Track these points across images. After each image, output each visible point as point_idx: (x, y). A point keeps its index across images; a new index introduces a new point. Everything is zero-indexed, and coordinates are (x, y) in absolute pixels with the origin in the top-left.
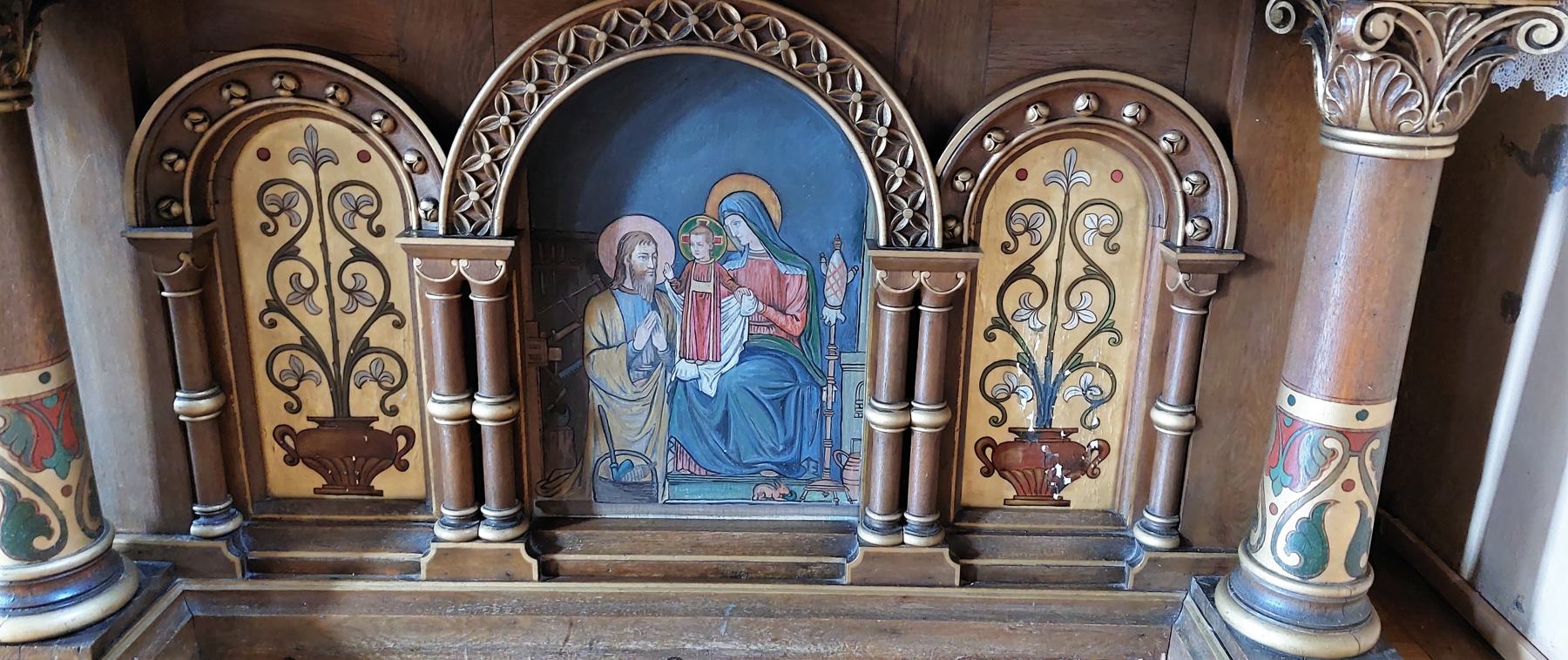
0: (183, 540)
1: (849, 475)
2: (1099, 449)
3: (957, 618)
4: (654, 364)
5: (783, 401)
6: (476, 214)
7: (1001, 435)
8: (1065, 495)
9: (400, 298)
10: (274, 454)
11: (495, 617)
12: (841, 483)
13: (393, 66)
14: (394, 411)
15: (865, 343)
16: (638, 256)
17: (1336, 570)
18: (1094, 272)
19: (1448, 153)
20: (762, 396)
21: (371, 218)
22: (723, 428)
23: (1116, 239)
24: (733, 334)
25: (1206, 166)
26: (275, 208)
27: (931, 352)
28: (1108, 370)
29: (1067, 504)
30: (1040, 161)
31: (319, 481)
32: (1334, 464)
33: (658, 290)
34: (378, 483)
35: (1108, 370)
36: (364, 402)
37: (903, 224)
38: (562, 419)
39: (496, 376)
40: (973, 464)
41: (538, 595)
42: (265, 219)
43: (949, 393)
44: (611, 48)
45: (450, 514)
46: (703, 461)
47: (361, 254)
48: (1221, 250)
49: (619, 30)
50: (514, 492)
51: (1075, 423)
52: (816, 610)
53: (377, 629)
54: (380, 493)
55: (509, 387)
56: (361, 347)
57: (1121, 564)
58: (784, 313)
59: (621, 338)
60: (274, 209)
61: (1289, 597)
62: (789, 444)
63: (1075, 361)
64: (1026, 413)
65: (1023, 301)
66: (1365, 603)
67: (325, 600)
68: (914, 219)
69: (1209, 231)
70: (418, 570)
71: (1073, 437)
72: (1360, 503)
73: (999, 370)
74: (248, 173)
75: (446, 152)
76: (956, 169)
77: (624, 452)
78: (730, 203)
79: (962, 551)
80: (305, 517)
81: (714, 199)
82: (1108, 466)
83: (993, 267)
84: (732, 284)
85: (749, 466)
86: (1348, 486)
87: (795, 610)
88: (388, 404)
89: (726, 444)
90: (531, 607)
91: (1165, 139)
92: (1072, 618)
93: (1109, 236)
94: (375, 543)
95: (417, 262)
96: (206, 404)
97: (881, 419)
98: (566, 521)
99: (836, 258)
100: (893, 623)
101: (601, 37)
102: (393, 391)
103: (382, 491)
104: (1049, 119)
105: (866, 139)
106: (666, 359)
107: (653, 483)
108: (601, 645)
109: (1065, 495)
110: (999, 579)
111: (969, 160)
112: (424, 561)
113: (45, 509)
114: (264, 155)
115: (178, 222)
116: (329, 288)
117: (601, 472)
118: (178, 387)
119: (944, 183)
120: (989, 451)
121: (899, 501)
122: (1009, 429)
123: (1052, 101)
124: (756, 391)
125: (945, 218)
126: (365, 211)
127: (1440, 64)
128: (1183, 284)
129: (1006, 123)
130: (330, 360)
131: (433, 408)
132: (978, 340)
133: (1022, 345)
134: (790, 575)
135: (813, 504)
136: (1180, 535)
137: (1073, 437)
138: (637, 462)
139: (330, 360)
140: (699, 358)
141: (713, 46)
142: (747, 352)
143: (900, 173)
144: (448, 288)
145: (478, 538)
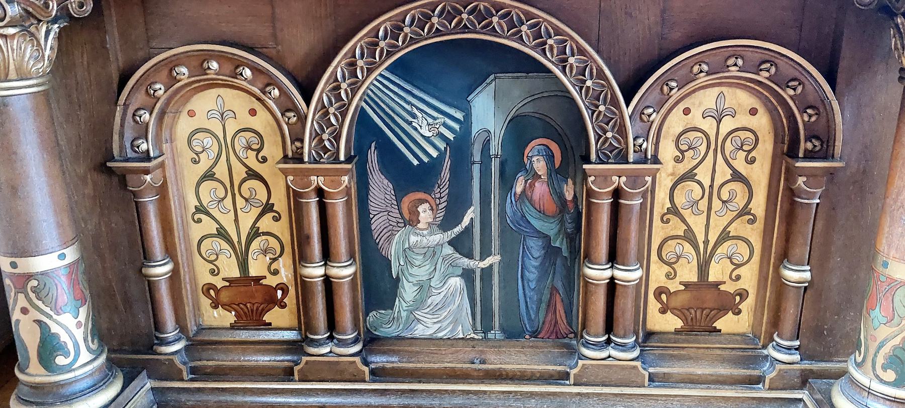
14: (276, 273)
21: (749, 152)
36: (717, 272)
70: (568, 378)
88: (273, 267)
91: (160, 89)
95: (290, 178)
103: (721, 330)
120: (664, 297)
122: (223, 279)
123: (199, 63)
128: (151, 182)
139: (235, 239)
141: (426, 39)
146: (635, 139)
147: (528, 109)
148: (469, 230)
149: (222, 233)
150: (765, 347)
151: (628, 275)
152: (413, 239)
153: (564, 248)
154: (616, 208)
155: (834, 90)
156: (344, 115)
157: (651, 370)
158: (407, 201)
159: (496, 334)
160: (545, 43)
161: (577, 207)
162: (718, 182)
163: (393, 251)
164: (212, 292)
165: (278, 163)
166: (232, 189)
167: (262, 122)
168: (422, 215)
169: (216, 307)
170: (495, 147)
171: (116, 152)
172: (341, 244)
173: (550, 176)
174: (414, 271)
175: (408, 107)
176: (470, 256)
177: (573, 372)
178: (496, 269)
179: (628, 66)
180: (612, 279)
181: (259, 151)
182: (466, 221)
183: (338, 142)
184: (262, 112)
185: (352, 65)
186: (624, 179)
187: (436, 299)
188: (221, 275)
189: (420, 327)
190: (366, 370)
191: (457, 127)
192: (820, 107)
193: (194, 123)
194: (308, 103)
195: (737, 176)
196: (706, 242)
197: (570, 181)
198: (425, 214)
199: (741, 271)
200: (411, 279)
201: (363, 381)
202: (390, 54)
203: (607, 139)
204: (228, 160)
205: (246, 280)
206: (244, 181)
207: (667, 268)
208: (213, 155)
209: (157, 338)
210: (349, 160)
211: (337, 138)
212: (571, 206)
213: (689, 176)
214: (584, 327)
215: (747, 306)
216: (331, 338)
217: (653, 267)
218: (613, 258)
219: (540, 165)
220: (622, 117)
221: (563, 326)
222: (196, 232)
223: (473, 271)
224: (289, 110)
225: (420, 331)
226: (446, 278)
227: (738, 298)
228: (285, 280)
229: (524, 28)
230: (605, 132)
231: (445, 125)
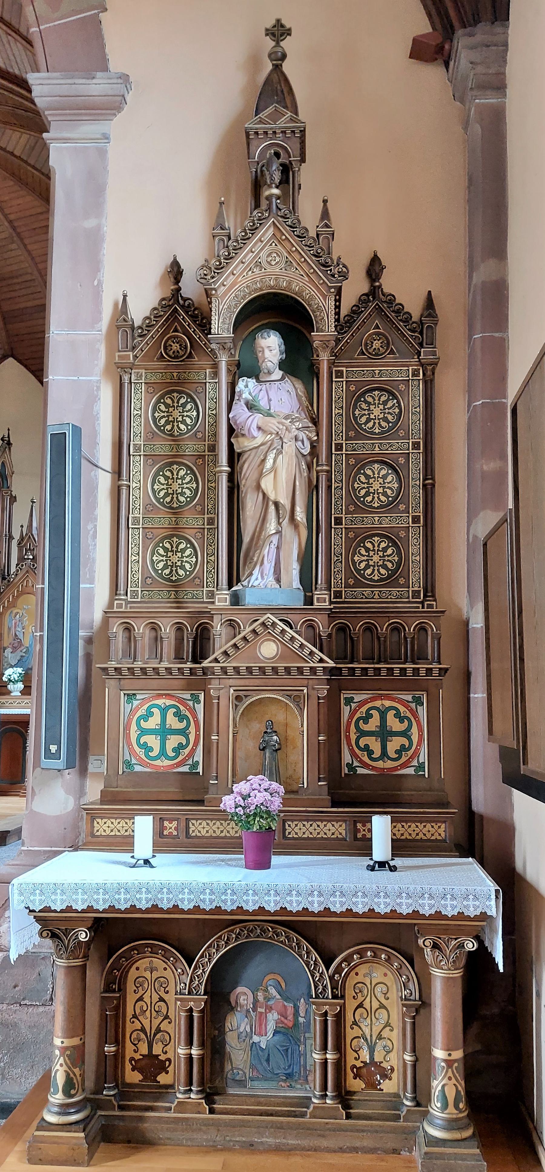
0: (100, 1097)
1: (310, 1078)
2: (391, 1069)
3: (343, 1131)
4: (246, 1037)
5: (287, 1050)
6: (197, 987)
7: (359, 1064)
8: (382, 1087)
9: (171, 1014)
10: (128, 1067)
11: (195, 1127)
12: (307, 1081)
13: (176, 944)
15: (312, 1030)
16: (242, 1000)
17: (451, 1108)
18: (382, 1006)
19: (461, 974)
20: (280, 1048)
21: (165, 988)
22: (268, 1060)
23: (388, 995)
24: (271, 1026)
25: (408, 973)
26: (138, 984)
27: (332, 1033)
28: (390, 1040)
29: (382, 1090)
30: (363, 970)
31: (141, 1077)
32: (445, 1071)
33: (248, 1011)
34: (159, 1078)
35: (390, 1040)
36: (157, 1049)
37: (320, 991)
38: (217, 1056)
39: (198, 1040)
40: (350, 1075)
41: (208, 1119)
42: (135, 988)
43: (339, 1048)
44: (237, 938)
45: (182, 1089)
46: (261, 1072)
47: (161, 999)
48: (415, 1000)
49: (239, 934)
50: (201, 1083)
51: (382, 1060)
52: (299, 1127)
53: (158, 1130)
54: (159, 1082)
55: (202, 1045)
56: (158, 1030)
57: (400, 1112)
58: (286, 1018)
59: (236, 1027)
60: (138, 985)
61: (443, 1119)
62: (289, 1066)
63: (380, 1037)
64: (366, 1055)
65: (361, 1015)
66: (466, 1121)
67: (141, 1119)
68: (323, 989)
69: (411, 994)
71: (381, 1065)
73: (356, 1040)
74: (133, 974)
75: (190, 969)
76: (336, 972)
77: (236, 1068)
78: (270, 983)
79: (346, 1106)
80: (136, 1090)
81: (265, 981)
82: (394, 1076)
83: (351, 1005)
84: (270, 1009)
85: (277, 1074)
87: (290, 1127)
89: (269, 1066)
90: (206, 1123)
92: (382, 1132)
93: (385, 994)
94: (157, 1100)
96: (113, 1049)
97: (317, 1056)
98: (218, 1094)
99: (302, 1000)
100: (322, 1132)
101: (234, 936)
102: (166, 1045)
104: (360, 958)
105: (308, 964)
106: (249, 1034)
107: (245, 1080)
108: (228, 1138)
109: (382, 1087)
110: (359, 1117)
111: (339, 970)
112: (173, 1106)
113: (75, 1081)
114: (137, 969)
115: (114, 991)
116: (151, 1010)
117: (229, 1076)
118: (106, 1043)
119: (331, 978)
120: (355, 1070)
121: (324, 1088)
123: (361, 953)
124: (278, 1047)
125: (332, 989)
126: (164, 986)
127: (448, 952)
129: (348, 959)
130: (149, 1035)
131: (180, 1051)
132: (348, 1029)
133: (362, 1031)
134: (289, 1114)
135: (297, 1089)
136: (417, 1101)
137: (381, 1065)
138: (240, 1072)
139: (149, 1035)
140: (260, 1035)
142: (276, 1032)
143: (318, 975)
144: (187, 1011)
145: (190, 1098)
165: (102, 993)
188: (361, 1059)
199: (167, 1048)
213: (141, 999)
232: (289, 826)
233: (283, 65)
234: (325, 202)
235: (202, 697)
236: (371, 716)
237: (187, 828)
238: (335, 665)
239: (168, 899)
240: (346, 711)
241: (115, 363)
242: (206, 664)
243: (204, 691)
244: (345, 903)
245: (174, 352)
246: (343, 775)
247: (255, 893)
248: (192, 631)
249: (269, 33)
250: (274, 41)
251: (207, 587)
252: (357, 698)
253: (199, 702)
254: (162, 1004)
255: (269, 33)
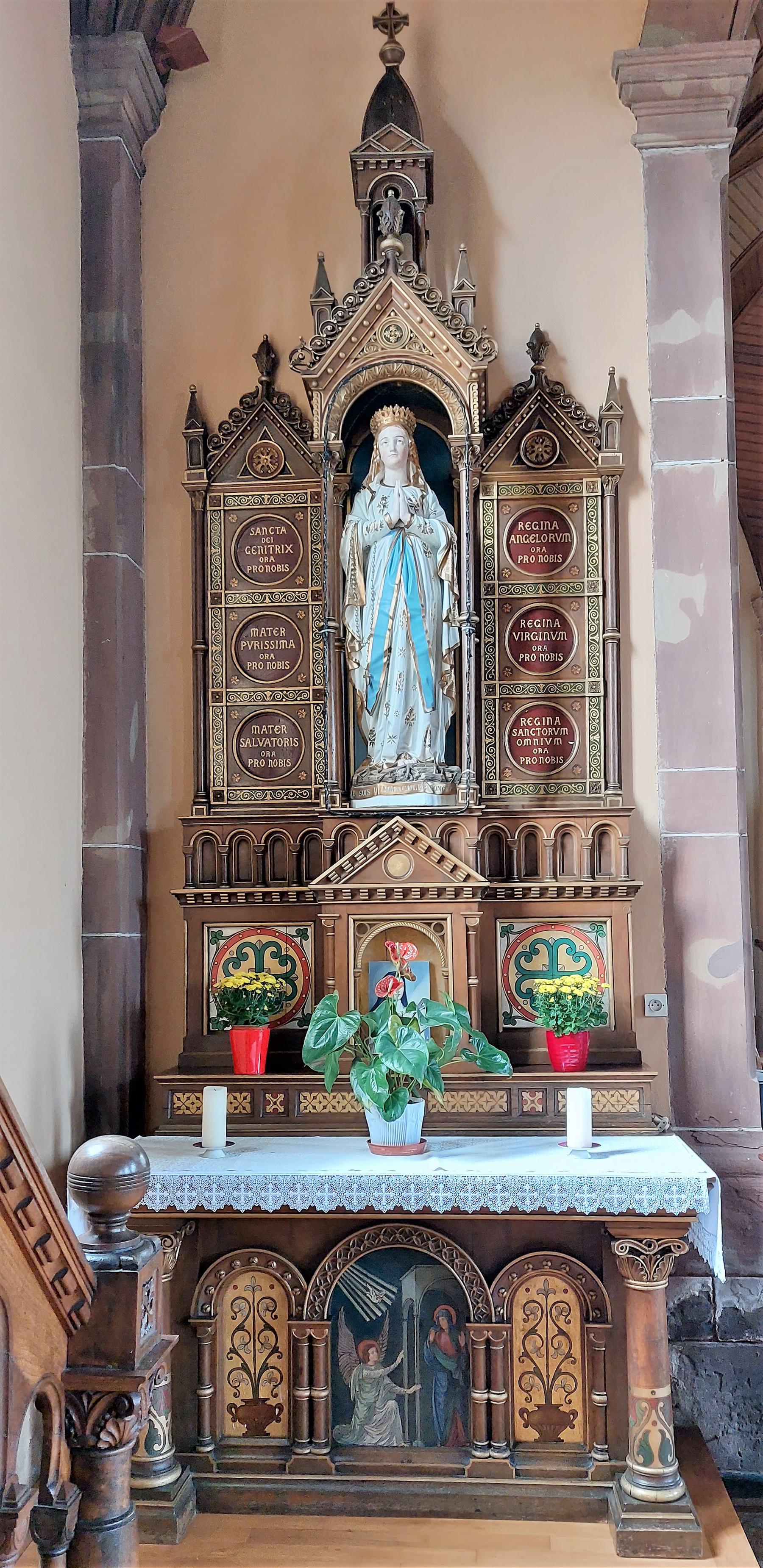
14: (276, 1396)
21: (567, 1316)
70: (587, 1476)
72: (662, 1433)
74: (521, 1297)
86: (654, 1423)
120: (525, 1415)
139: (252, 1372)
146: (495, 1308)
147: (436, 1287)
148: (400, 1366)
149: (245, 1367)
150: (590, 1452)
151: (498, 1397)
152: (365, 1372)
153: (461, 1379)
154: (488, 1351)
155: (602, 1281)
156: (328, 1291)
157: (518, 1467)
158: (361, 1346)
159: (418, 1442)
160: (441, 1251)
161: (467, 1350)
162: (550, 1336)
163: (352, 1381)
164: (233, 1410)
166: (254, 1337)
167: (276, 1293)
168: (371, 1355)
169: (234, 1421)
170: (416, 1311)
171: (192, 1313)
172: (320, 1376)
173: (450, 1329)
174: (364, 1396)
175: (364, 1284)
176: (401, 1385)
177: (467, 1468)
178: (418, 1395)
179: (489, 1263)
180: (489, 1400)
181: (273, 1311)
182: (399, 1360)
183: (324, 1307)
184: (278, 1288)
185: (334, 1261)
186: (490, 1333)
187: (378, 1417)
188: (241, 1398)
189: (368, 1437)
190: (333, 1466)
191: (393, 1297)
192: (595, 1289)
193: (237, 1293)
194: (308, 1284)
195: (561, 1332)
196: (548, 1376)
197: (462, 1333)
198: (373, 1354)
199: (572, 1397)
200: (363, 1401)
201: (330, 1474)
202: (356, 1256)
203: (479, 1308)
204: (254, 1317)
205: (256, 1401)
206: (262, 1331)
207: (526, 1395)
208: (245, 1314)
209: (198, 1441)
210: (328, 1319)
211: (323, 1304)
212: (464, 1350)
213: (533, 1331)
214: (474, 1437)
215: (578, 1421)
216: (310, 1443)
217: (516, 1393)
218: (489, 1386)
219: (444, 1323)
220: (487, 1296)
221: (462, 1439)
222: (228, 1365)
223: (403, 1396)
224: (296, 1287)
225: (368, 1440)
226: (385, 1401)
227: (572, 1416)
228: (281, 1401)
229: (430, 1242)
230: (478, 1303)
231: (386, 1295)
232: (305, 1098)
233: (400, 66)
234: (321, 261)
235: (310, 932)
236: (537, 952)
237: (509, 1102)
238: (488, 884)
239: (359, 1198)
240: (501, 944)
241: (183, 484)
242: (314, 885)
243: (314, 922)
244: (508, 1199)
245: (537, 456)
246: (501, 1030)
247: (447, 1188)
248: (259, 842)
249: (377, 23)
250: (386, 34)
251: (316, 784)
252: (228, 932)
253: (306, 938)
254: (560, 1338)
255: (377, 23)
